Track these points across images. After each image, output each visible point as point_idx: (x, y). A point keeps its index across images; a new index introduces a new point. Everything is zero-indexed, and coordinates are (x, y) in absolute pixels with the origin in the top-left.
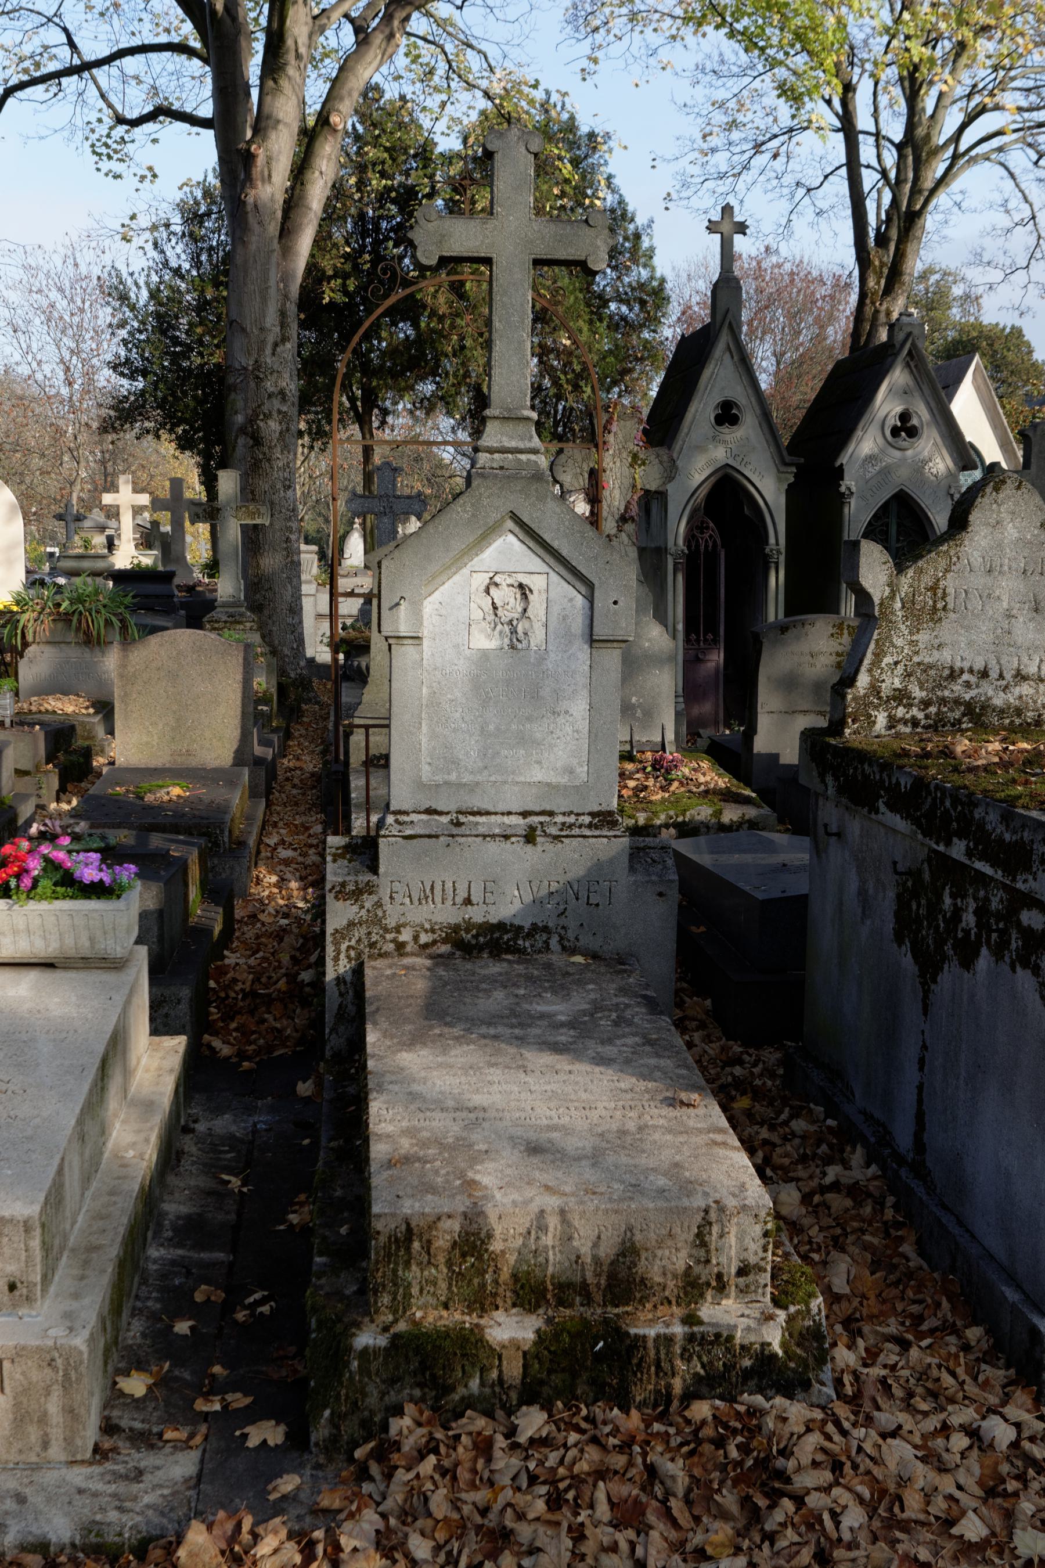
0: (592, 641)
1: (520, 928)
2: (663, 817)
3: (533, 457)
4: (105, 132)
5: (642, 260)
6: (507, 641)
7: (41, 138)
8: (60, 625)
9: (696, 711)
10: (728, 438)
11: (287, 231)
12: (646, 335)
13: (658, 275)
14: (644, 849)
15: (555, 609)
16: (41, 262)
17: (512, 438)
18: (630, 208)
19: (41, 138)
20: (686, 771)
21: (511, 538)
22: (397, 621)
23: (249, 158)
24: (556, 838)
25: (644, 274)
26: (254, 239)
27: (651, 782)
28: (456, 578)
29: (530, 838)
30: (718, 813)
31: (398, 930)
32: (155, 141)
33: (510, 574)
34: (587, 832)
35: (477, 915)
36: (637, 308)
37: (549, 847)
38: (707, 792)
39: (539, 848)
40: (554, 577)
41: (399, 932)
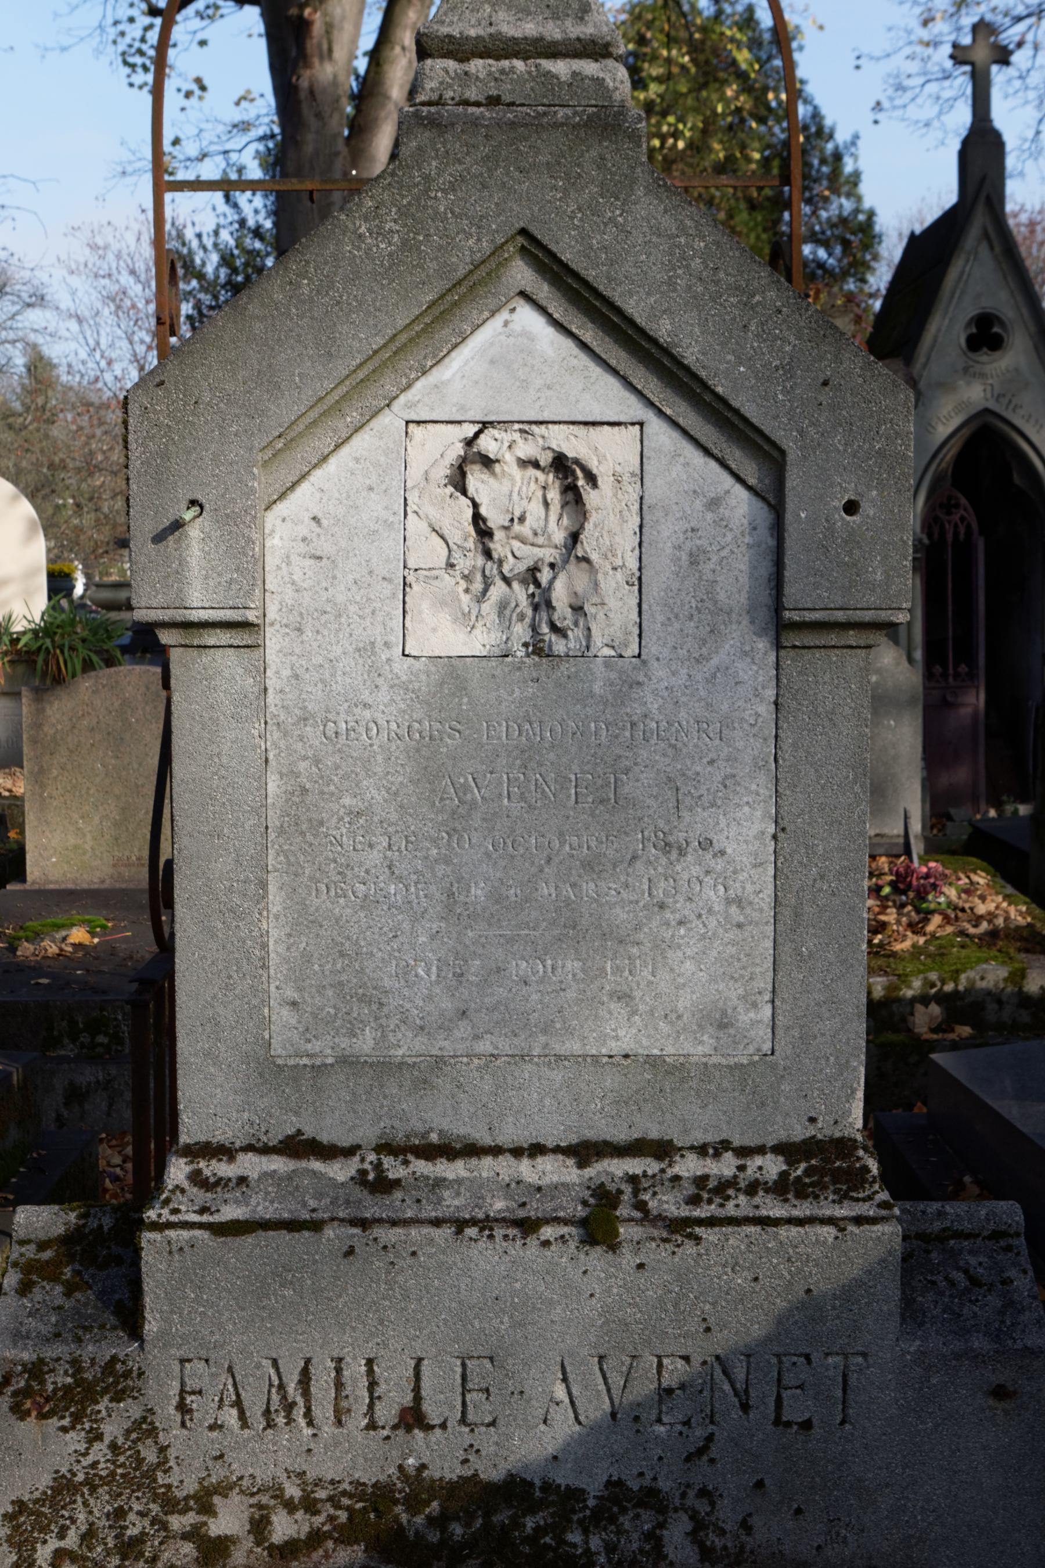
0: (783, 625)
1: (575, 1494)
2: (917, 984)
3: (589, 67)
4: (138, 34)
5: (845, 189)
6: (521, 632)
7: (64, 49)
8: (21, 669)
9: (945, 780)
10: (987, 369)
11: (360, 128)
12: (851, 285)
13: (867, 204)
14: (942, 1237)
15: (667, 532)
16: (110, 239)
17: (525, 12)
18: (828, 122)
19: (64, 49)
20: (952, 893)
21: (527, 318)
22: (179, 574)
23: (302, 27)
24: (680, 1227)
25: (848, 205)
26: (310, 137)
27: (890, 916)
28: (361, 442)
29: (597, 1226)
30: (1018, 976)
31: (204, 1502)
32: (203, 43)
33: (527, 426)
34: (776, 1210)
35: (440, 1456)
36: (838, 250)
37: (657, 1254)
38: (993, 934)
39: (628, 1258)
40: (659, 431)
41: (207, 1509)
